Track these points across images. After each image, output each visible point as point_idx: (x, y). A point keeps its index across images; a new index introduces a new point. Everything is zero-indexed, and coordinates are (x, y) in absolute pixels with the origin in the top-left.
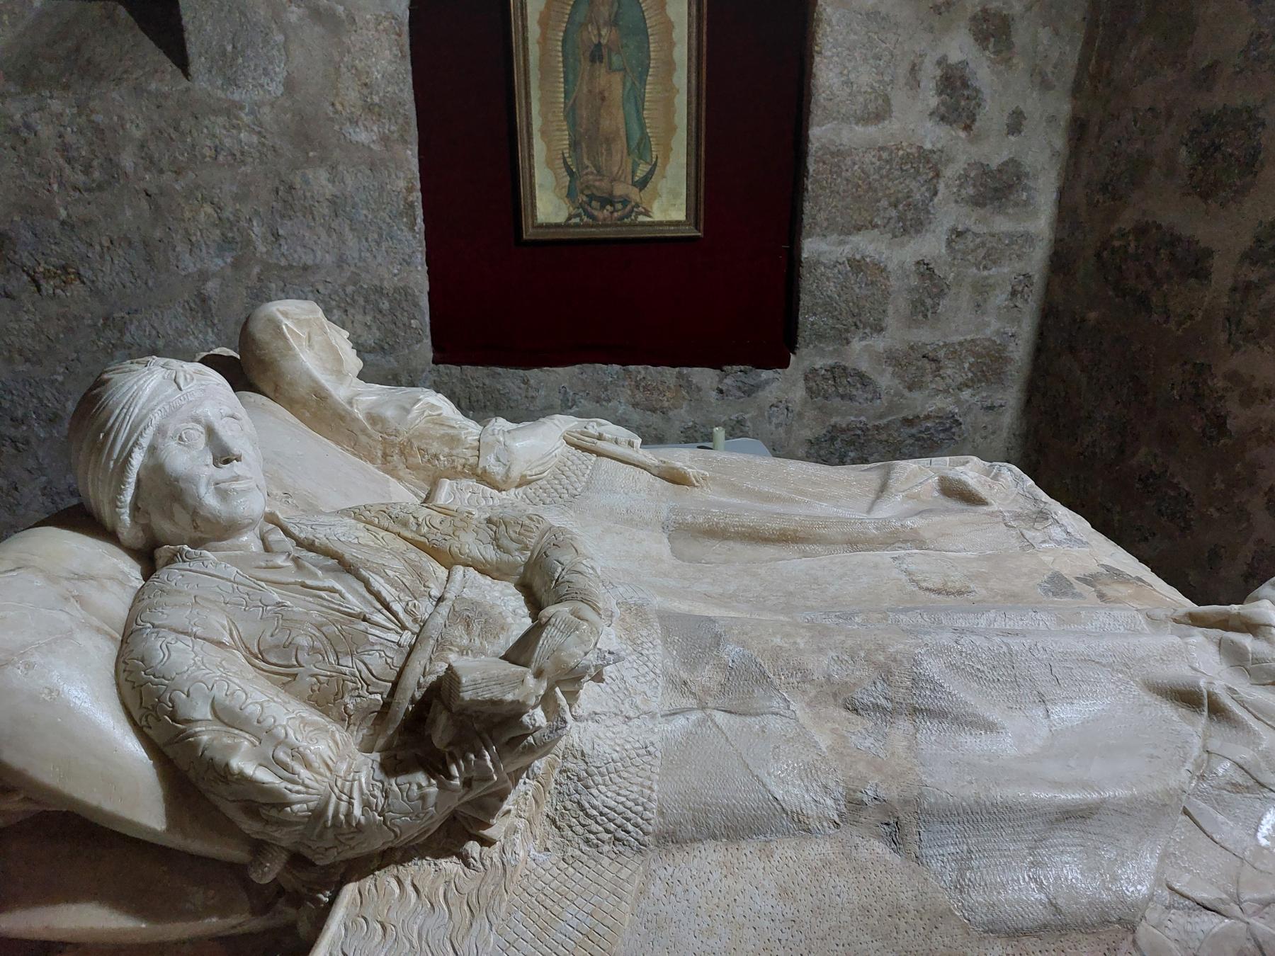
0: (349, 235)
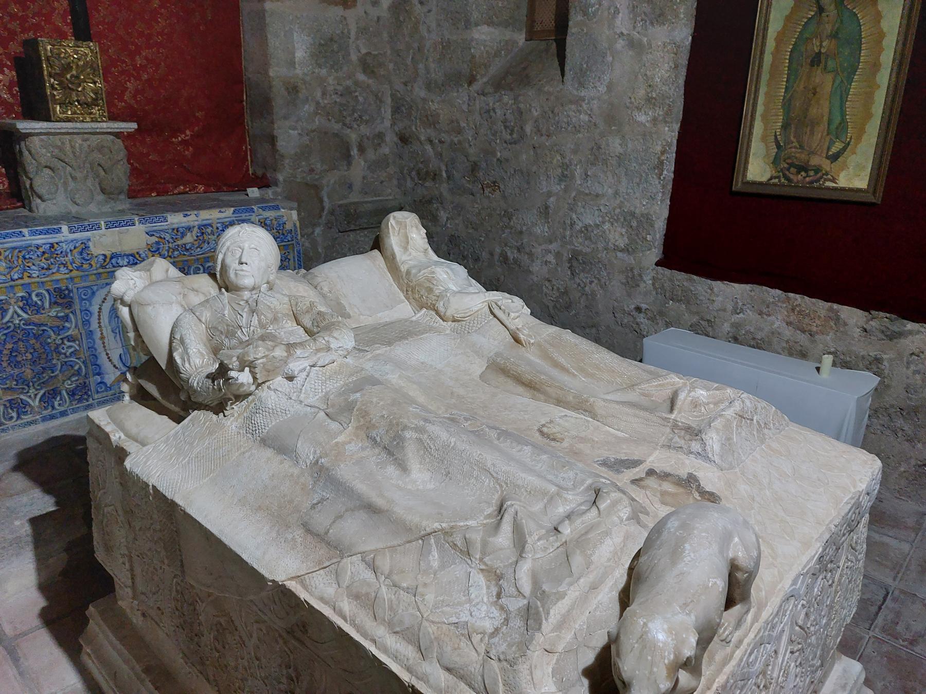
0: (624, 180)
